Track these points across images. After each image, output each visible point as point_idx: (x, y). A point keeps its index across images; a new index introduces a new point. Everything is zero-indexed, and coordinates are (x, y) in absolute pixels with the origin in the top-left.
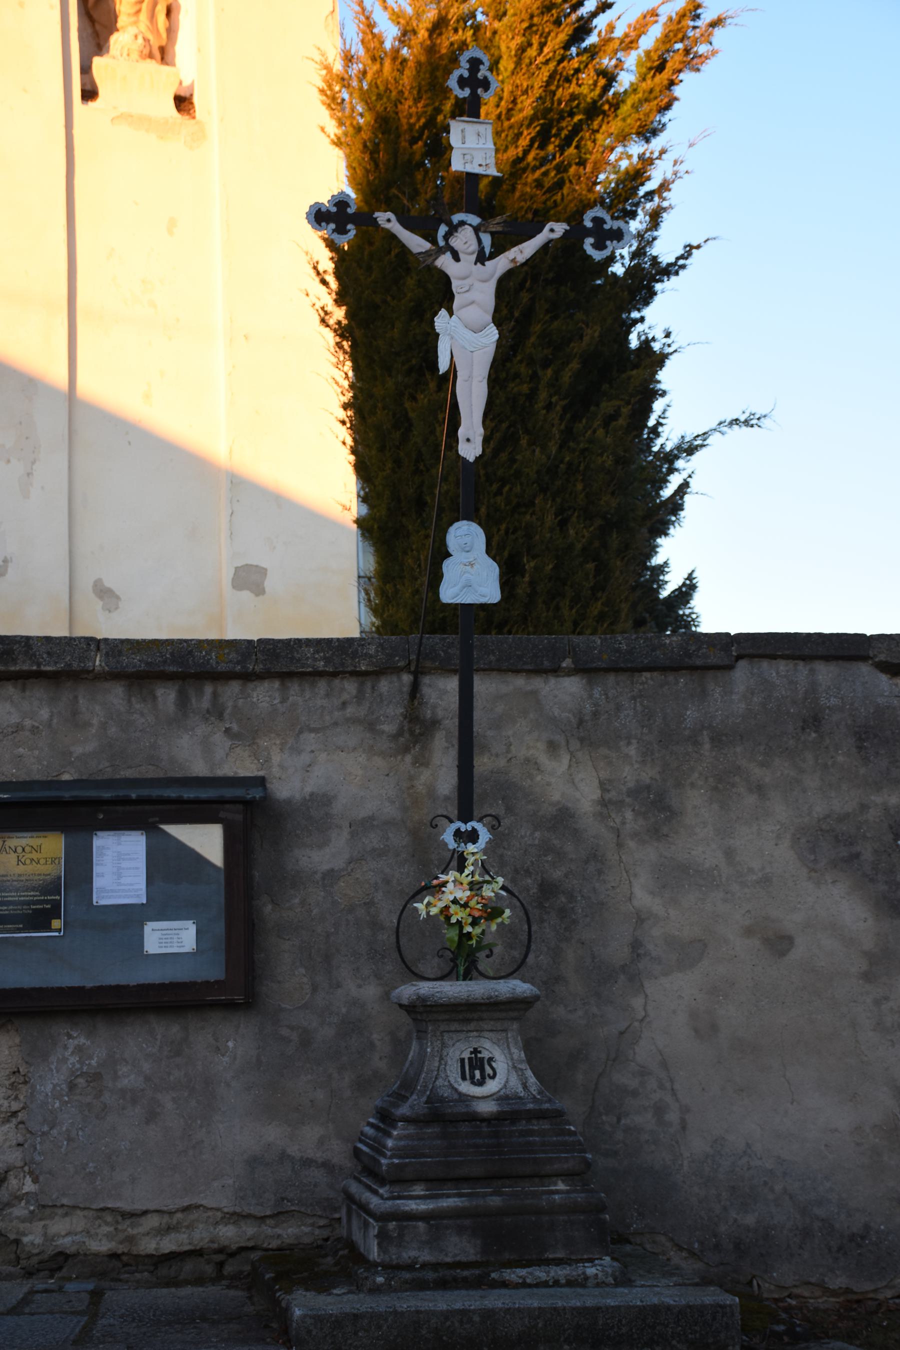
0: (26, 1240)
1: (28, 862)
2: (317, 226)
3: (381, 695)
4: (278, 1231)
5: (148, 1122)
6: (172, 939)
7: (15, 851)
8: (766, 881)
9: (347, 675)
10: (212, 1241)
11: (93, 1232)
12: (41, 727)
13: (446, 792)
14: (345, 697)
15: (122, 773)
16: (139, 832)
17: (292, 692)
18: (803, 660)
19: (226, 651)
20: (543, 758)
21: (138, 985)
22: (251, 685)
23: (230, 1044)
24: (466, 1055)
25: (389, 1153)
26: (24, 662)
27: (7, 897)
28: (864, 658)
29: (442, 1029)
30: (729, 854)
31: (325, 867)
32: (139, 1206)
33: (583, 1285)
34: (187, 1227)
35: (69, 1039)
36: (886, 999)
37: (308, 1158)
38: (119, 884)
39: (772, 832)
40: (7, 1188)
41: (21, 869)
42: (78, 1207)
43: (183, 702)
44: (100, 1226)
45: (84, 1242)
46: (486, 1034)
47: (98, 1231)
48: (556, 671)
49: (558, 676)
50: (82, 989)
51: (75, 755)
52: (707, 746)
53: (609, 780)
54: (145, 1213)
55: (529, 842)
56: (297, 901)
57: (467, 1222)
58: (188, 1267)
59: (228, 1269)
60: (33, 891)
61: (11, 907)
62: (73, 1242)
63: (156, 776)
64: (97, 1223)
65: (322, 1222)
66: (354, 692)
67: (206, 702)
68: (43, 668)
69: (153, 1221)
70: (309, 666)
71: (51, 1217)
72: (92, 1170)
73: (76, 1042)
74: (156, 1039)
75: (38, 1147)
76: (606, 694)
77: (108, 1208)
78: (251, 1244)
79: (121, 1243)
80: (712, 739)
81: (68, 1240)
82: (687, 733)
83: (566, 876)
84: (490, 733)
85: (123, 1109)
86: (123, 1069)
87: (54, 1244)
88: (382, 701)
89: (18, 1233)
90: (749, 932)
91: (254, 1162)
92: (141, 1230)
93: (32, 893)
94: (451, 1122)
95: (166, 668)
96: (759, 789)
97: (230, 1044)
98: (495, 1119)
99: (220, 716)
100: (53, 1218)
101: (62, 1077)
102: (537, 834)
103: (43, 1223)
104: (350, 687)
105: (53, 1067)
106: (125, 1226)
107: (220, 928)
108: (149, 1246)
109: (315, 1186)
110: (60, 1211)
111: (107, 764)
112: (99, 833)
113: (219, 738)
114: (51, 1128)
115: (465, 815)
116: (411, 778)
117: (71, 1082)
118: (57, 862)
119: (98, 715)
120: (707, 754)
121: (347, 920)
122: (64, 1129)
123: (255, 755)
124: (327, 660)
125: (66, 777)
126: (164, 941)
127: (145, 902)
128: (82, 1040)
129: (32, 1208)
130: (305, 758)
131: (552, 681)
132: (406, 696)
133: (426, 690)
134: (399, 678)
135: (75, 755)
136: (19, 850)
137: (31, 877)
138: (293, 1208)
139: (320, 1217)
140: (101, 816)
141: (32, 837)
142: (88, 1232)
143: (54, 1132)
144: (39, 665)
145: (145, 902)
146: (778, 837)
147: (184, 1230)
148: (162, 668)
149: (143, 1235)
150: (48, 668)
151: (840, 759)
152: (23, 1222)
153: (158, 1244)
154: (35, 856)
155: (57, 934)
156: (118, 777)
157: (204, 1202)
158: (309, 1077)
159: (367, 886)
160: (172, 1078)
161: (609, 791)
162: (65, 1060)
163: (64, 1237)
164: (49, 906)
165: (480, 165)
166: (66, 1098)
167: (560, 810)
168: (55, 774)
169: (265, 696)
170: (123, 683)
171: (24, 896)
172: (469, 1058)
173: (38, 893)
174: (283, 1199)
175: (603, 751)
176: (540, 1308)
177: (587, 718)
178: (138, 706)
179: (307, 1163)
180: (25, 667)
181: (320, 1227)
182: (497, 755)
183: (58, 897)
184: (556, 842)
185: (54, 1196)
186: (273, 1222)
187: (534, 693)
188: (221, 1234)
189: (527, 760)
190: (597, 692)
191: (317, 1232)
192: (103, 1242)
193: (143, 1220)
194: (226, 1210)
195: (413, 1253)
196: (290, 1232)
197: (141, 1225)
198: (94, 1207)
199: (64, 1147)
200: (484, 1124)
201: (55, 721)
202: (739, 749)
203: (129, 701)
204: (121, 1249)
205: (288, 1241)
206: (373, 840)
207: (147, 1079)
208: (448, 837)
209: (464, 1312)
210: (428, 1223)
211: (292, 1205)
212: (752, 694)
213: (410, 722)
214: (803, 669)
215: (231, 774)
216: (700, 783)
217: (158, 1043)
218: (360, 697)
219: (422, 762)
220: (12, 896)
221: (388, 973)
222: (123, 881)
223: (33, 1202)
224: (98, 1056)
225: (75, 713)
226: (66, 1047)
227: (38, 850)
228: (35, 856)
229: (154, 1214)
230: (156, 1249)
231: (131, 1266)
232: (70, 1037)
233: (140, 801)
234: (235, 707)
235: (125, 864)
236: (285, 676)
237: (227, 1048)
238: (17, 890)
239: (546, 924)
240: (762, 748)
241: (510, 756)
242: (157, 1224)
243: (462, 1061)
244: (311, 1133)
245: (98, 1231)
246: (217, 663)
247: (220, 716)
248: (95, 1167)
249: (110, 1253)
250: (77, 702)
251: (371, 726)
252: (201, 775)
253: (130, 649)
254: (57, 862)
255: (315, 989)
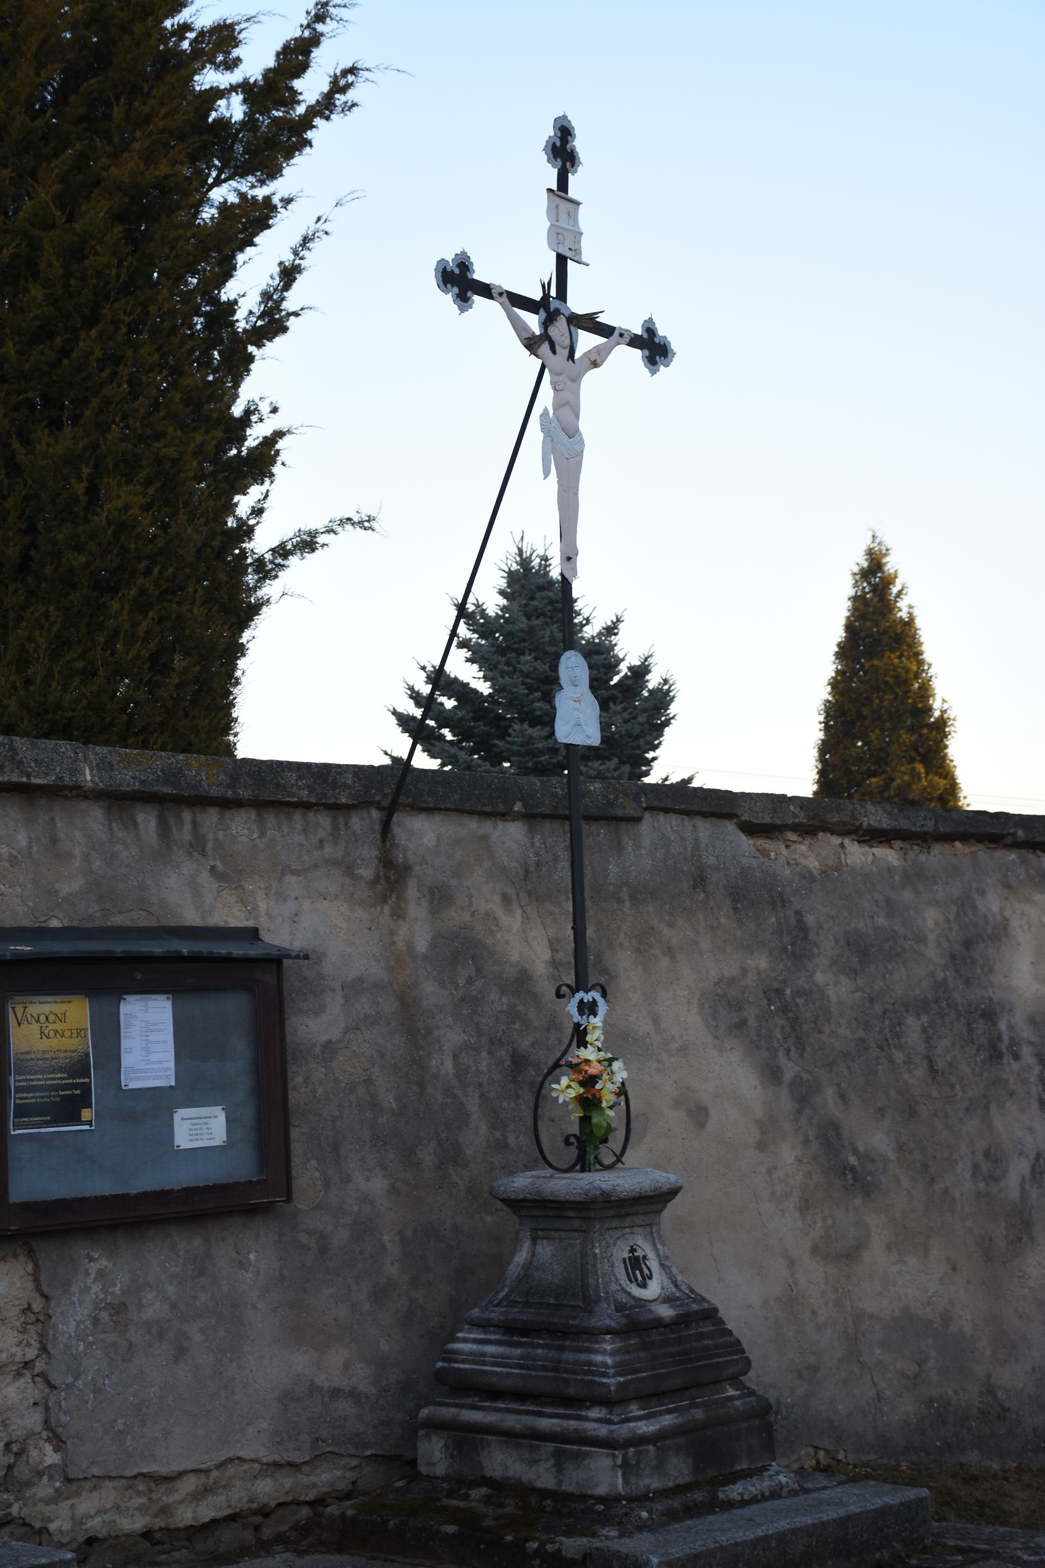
0: (53, 1527)
1: (52, 1034)
2: (441, 284)
3: (354, 833)
4: (313, 1478)
5: (176, 1360)
6: (202, 1129)
7: (38, 1021)
8: (684, 1048)
9: (322, 808)
10: (251, 1501)
11: (123, 1506)
12: (20, 857)
13: (424, 950)
14: (322, 833)
15: (113, 919)
16: (165, 996)
17: (269, 825)
18: (688, 815)
19: (215, 771)
20: (500, 912)
21: (184, 1189)
22: (228, 814)
23: (252, 1256)
24: (626, 1255)
25: (612, 1371)
26: (12, 771)
27: (32, 1080)
28: (730, 816)
29: (606, 1227)
30: (656, 1020)
31: (323, 1038)
32: (175, 1467)
33: (779, 1496)
34: (224, 1487)
35: (90, 1262)
36: (775, 1168)
37: (335, 1388)
38: (148, 1062)
39: (684, 997)
40: (27, 1461)
41: (45, 1044)
42: (110, 1478)
43: (164, 831)
44: (131, 1498)
45: (114, 1521)
46: (637, 1230)
47: (129, 1504)
48: (504, 815)
49: (505, 821)
50: (125, 1197)
51: (61, 895)
52: (628, 904)
53: (556, 939)
54: (180, 1474)
55: (499, 1008)
56: (300, 1079)
57: (682, 1440)
58: (227, 1536)
59: (267, 1533)
60: (60, 1072)
61: (38, 1094)
62: (104, 1522)
63: (148, 924)
64: (127, 1495)
65: (354, 1462)
66: (329, 828)
67: (186, 834)
68: (34, 781)
69: (189, 1485)
70: (294, 796)
71: (78, 1494)
72: (121, 1427)
73: (98, 1265)
74: (179, 1256)
75: (63, 1404)
76: (545, 843)
77: (141, 1474)
78: (289, 1499)
79: (156, 1516)
80: (631, 896)
81: (97, 1520)
82: (611, 889)
83: (533, 1045)
84: (453, 882)
85: (150, 1346)
86: (148, 1296)
87: (84, 1527)
88: (356, 841)
89: (43, 1520)
90: (677, 1103)
91: (287, 1398)
92: (177, 1497)
93: (59, 1076)
94: (644, 1330)
95: (161, 788)
96: (669, 951)
97: (252, 1256)
98: (675, 1324)
99: (203, 853)
100: (80, 1495)
101: (86, 1312)
102: (505, 999)
103: (69, 1502)
104: (324, 821)
105: (75, 1299)
106: (160, 1495)
107: (247, 1114)
108: (186, 1516)
109: (345, 1420)
110: (88, 1485)
111: (97, 908)
112: (129, 998)
113: (205, 877)
114: (76, 1379)
115: (581, 984)
116: (392, 933)
117: (95, 1317)
118: (82, 1033)
119: (79, 844)
120: (628, 912)
121: (349, 1101)
122: (90, 1378)
123: (242, 902)
124: (311, 789)
125: (55, 923)
126: (194, 1132)
127: (173, 1084)
128: (104, 1263)
129: (58, 1484)
130: (291, 906)
131: (500, 825)
132: (378, 836)
133: (396, 830)
134: (369, 813)
135: (61, 895)
136: (43, 1019)
137: (57, 1055)
138: (328, 1449)
139: (351, 1456)
140: (139, 976)
141: (56, 1002)
142: (118, 1508)
143: (80, 1383)
144: (29, 776)
145: (173, 1084)
146: (689, 1003)
147: (221, 1490)
148: (156, 788)
149: (180, 1503)
150: (40, 781)
151: (723, 920)
152: (48, 1504)
153: (195, 1512)
154: (59, 1026)
155: (87, 1127)
156: (110, 924)
157: (241, 1454)
158: (331, 1291)
159: (364, 1060)
160: (198, 1304)
161: (557, 951)
162: (86, 1289)
163: (92, 1517)
164: (78, 1092)
165: (570, 249)
166: (91, 1339)
167: (519, 972)
168: (42, 919)
169: (243, 828)
170: (102, 804)
171: (51, 1079)
172: (629, 1258)
173: (65, 1075)
174: (317, 1439)
175: (548, 906)
176: (814, 1524)
177: (532, 869)
178: (120, 834)
179: (336, 1393)
180: (14, 779)
181: (351, 1469)
182: (462, 909)
183: (87, 1080)
184: (520, 1007)
185: (84, 1466)
186: (308, 1469)
187: (485, 838)
188: (259, 1491)
189: (488, 914)
190: (537, 838)
191: (348, 1474)
192: (136, 1518)
193: (178, 1484)
194: (265, 1460)
195: (647, 1481)
196: (326, 1478)
197: (177, 1490)
198: (127, 1474)
199: (90, 1402)
200: (667, 1330)
201: (35, 849)
202: (651, 908)
203: (111, 828)
204: (158, 1523)
205: (323, 1490)
206: (364, 1006)
207: (173, 1306)
208: (572, 1007)
209: (765, 1538)
210: (655, 1445)
211: (327, 1445)
212: (656, 849)
213: (384, 866)
214: (688, 823)
215: (222, 924)
216: (627, 943)
217: (181, 1261)
218: (335, 835)
219: (399, 914)
220: (38, 1080)
221: (391, 1162)
222: (154, 1057)
223: (57, 1477)
224: (121, 1282)
225: (54, 840)
226: (87, 1274)
227: (61, 1018)
228: (59, 1026)
229: (191, 1475)
230: (194, 1518)
231: (163, 1544)
232: (91, 1259)
233: (194, 959)
234: (216, 840)
235: (153, 1037)
236: (260, 805)
237: (248, 1260)
238: (43, 1071)
239: (521, 1101)
240: (668, 906)
241: (472, 909)
242: (193, 1488)
243: (624, 1260)
244: (337, 1356)
245: (129, 1504)
246: (209, 785)
247: (203, 853)
248: (125, 1424)
249: (145, 1530)
250: (55, 826)
251: (350, 871)
252: (193, 924)
253: (120, 762)
254: (82, 1033)
255: (327, 1185)
